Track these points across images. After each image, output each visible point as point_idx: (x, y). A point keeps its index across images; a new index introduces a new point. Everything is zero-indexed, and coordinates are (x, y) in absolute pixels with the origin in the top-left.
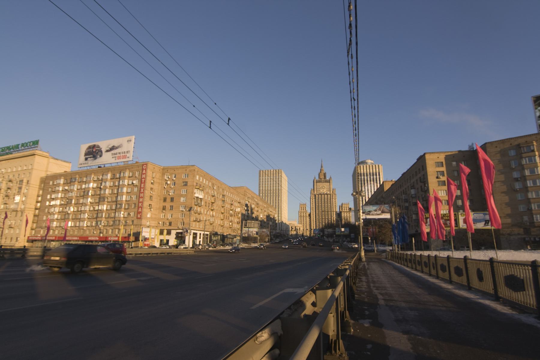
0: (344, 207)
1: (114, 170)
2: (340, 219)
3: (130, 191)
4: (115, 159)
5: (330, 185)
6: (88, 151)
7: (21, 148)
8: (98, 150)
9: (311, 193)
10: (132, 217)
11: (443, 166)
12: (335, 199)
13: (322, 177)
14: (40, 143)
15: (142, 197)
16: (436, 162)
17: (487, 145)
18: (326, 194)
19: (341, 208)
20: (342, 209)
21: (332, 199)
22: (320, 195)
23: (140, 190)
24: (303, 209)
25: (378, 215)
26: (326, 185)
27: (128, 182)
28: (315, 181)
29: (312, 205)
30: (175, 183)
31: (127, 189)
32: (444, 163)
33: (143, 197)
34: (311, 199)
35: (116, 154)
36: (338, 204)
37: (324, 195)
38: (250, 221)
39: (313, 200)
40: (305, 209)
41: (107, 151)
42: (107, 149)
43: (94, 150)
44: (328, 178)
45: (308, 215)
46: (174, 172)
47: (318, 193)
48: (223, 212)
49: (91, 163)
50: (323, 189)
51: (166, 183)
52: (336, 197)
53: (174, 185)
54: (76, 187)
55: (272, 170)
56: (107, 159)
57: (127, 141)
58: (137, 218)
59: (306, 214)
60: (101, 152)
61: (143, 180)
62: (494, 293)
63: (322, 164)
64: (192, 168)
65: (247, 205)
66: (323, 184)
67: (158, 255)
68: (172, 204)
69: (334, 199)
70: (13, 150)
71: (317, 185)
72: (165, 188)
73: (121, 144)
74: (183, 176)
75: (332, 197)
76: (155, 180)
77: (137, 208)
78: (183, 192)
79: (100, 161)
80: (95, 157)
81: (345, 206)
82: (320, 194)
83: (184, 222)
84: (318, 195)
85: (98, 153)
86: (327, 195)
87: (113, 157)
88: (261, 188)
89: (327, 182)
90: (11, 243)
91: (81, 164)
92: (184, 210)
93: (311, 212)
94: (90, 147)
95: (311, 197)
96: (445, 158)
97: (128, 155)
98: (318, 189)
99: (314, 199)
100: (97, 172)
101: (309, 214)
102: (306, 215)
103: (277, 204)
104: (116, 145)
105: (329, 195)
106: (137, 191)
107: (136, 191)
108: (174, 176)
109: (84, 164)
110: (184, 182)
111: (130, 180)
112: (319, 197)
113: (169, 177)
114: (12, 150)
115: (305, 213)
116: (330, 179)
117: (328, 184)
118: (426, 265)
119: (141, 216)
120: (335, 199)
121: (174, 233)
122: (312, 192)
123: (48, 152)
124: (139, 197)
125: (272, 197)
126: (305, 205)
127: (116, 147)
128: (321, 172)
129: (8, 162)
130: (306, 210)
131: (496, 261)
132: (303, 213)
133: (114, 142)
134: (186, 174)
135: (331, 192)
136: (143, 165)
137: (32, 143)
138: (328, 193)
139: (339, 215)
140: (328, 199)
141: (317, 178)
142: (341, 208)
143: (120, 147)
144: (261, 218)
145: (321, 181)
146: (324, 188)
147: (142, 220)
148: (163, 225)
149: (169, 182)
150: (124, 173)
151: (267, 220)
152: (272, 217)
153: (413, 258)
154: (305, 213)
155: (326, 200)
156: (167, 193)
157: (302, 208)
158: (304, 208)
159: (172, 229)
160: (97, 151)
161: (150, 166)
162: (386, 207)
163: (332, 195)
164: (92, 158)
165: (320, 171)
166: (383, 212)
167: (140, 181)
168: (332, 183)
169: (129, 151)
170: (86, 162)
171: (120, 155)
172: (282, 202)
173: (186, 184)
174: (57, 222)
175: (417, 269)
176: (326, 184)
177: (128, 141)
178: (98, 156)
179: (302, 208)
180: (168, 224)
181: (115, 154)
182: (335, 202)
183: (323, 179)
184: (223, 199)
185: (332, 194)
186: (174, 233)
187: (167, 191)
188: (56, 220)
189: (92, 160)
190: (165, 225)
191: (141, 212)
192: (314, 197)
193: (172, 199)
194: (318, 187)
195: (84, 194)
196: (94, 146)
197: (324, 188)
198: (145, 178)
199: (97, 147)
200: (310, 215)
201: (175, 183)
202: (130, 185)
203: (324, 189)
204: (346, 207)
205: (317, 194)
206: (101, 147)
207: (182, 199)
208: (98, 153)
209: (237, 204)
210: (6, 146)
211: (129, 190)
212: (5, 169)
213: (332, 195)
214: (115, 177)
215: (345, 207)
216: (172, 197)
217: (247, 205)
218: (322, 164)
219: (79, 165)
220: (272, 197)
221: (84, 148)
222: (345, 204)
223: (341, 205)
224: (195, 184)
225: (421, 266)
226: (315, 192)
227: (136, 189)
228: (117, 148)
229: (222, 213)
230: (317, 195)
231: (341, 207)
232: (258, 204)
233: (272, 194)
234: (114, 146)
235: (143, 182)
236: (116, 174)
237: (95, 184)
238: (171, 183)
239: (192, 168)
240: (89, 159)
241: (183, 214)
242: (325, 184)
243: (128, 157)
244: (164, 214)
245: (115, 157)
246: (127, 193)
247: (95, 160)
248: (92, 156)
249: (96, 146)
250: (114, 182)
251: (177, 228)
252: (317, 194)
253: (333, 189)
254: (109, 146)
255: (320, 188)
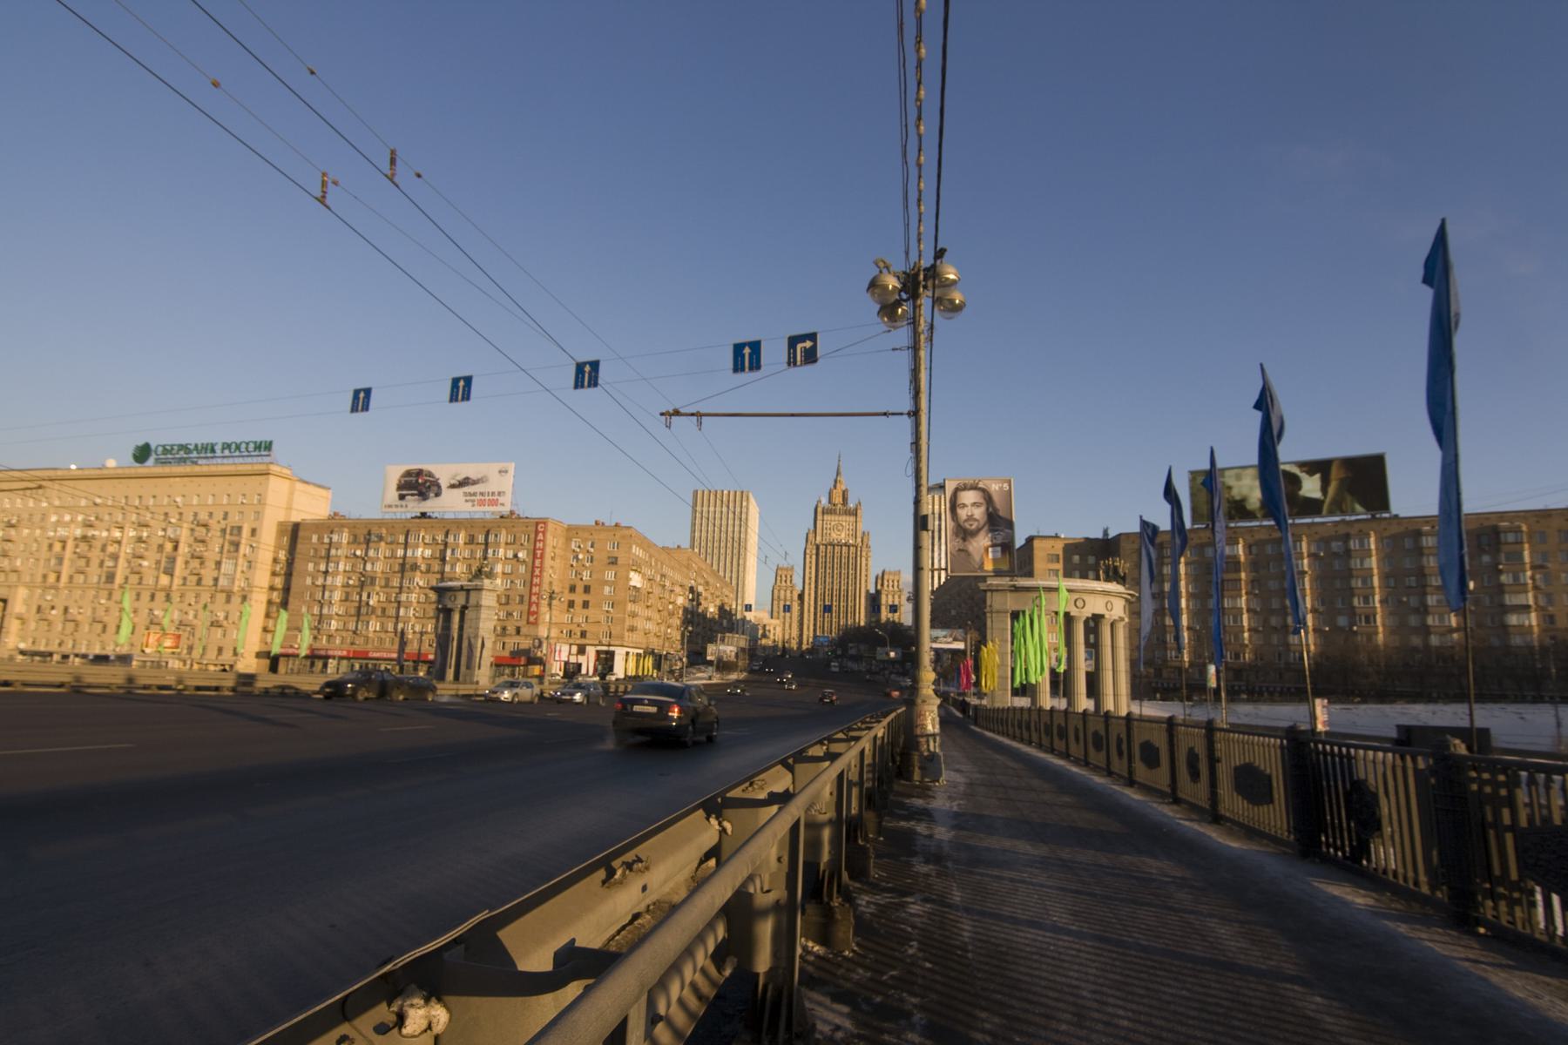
0: (888, 581)
1: (472, 527)
2: (944, 755)
3: (509, 572)
4: (473, 506)
5: (856, 522)
6: (405, 481)
7: (222, 452)
8: (431, 482)
9: (807, 541)
10: (517, 620)
11: (1058, 562)
12: (867, 560)
13: (838, 500)
14: (274, 447)
15: (536, 585)
16: (1049, 554)
17: (1122, 537)
18: (845, 545)
19: (880, 582)
20: (882, 585)
21: (859, 558)
22: (829, 547)
23: (533, 572)
24: (786, 581)
25: (949, 643)
26: (846, 521)
27: (505, 553)
28: (820, 510)
29: (807, 570)
30: (592, 557)
31: (504, 567)
32: (1061, 557)
33: (539, 585)
34: (808, 556)
35: (474, 494)
36: (874, 570)
37: (841, 546)
38: (731, 635)
39: (811, 557)
40: (791, 581)
41: (453, 486)
42: (453, 482)
43: (420, 481)
44: (851, 505)
45: (796, 597)
46: (591, 537)
47: (824, 542)
48: (661, 609)
49: (413, 507)
50: (839, 530)
51: (576, 557)
52: (870, 554)
53: (591, 562)
54: (384, 551)
55: (725, 492)
56: (450, 504)
57: (497, 471)
58: (528, 622)
59: (791, 592)
60: (439, 487)
61: (539, 552)
62: (1446, 900)
63: (839, 466)
64: (627, 532)
65: (692, 590)
66: (840, 518)
67: (221, 693)
68: (586, 597)
69: (863, 559)
70: (197, 455)
71: (823, 520)
72: (572, 566)
73: (485, 477)
74: (609, 547)
75: (859, 553)
76: (556, 551)
77: (526, 603)
78: (609, 575)
79: (432, 506)
80: (423, 496)
81: (891, 577)
82: (830, 545)
83: (610, 633)
84: (826, 546)
85: (429, 487)
86: (849, 546)
87: (467, 501)
88: (697, 534)
89: (850, 515)
90: (220, 658)
91: (390, 506)
92: (610, 609)
93: (804, 588)
94: (408, 473)
95: (808, 551)
96: (1064, 548)
97: (501, 500)
98: (825, 531)
99: (814, 557)
100: (432, 527)
101: (799, 592)
102: (791, 597)
103: (734, 576)
104: (473, 476)
105: (851, 548)
106: (526, 571)
107: (524, 572)
108: (590, 544)
109: (397, 506)
110: (609, 558)
111: (510, 549)
112: (826, 552)
113: (582, 546)
114: (195, 454)
115: (788, 592)
116: (857, 506)
117: (852, 519)
118: (1099, 742)
119: (536, 619)
120: (867, 560)
121: (591, 651)
122: (811, 536)
123: (289, 467)
124: (531, 585)
125: (722, 558)
126: (792, 568)
127: (474, 481)
128: (835, 487)
129: (192, 481)
130: (793, 582)
131: (1136, 717)
132: (785, 591)
133: (471, 471)
134: (614, 544)
135: (859, 540)
136: (537, 524)
137: (252, 446)
138: (851, 541)
139: (874, 601)
140: (848, 557)
141: (824, 501)
142: (880, 582)
143: (483, 482)
144: (711, 613)
145: (835, 510)
146: (840, 528)
147: (537, 627)
148: (570, 636)
149: (581, 556)
150: (496, 536)
151: (720, 616)
152: (728, 609)
153: (1034, 716)
154: (788, 592)
155: (843, 560)
156: (576, 575)
157: (784, 578)
158: (789, 576)
159: (589, 645)
160: (428, 484)
161: (550, 527)
162: (959, 633)
163: (859, 549)
164: (416, 497)
165: (833, 483)
166: (955, 639)
167: (532, 554)
168: (861, 517)
169: (504, 492)
170: (403, 503)
171: (483, 498)
172: (747, 569)
173: (613, 562)
174: (338, 621)
175: (1181, 795)
176: (848, 518)
177: (500, 472)
178: (432, 495)
179: (784, 578)
180: (579, 634)
181: (470, 494)
182: (867, 565)
183: (839, 506)
184: (662, 583)
185: (860, 544)
186: (591, 651)
187: (576, 572)
188: (336, 617)
189: (414, 500)
190: (573, 636)
191: (536, 613)
192: (814, 552)
193: (587, 589)
194: (825, 526)
195: (406, 567)
196: (420, 473)
197: (840, 528)
198: (543, 550)
199: (426, 475)
200: (801, 597)
201: (592, 557)
202: (509, 559)
203: (839, 530)
204: (893, 581)
205: (823, 545)
206: (437, 477)
207: (607, 589)
208: (429, 487)
209: (678, 589)
210: (177, 443)
211: (508, 569)
212: (184, 496)
213: (861, 548)
214: (475, 541)
215: (890, 581)
216: (586, 584)
217: (692, 590)
218: (839, 466)
219: (385, 506)
220: (722, 558)
221: (395, 474)
222: (890, 573)
223: (880, 575)
224: (631, 562)
225: (1064, 741)
226: (819, 538)
227: (522, 569)
228: (475, 483)
229: (659, 611)
230: (821, 547)
231: (881, 578)
232: (707, 583)
233: (722, 551)
234: (467, 478)
235: (539, 556)
236: (476, 535)
237: (427, 550)
238: (584, 558)
239: (627, 532)
240: (408, 498)
241: (608, 617)
242: (844, 518)
243: (503, 505)
244: (570, 616)
245: (473, 501)
246: (504, 573)
247: (424, 503)
248: (415, 492)
249: (424, 473)
250: (472, 551)
251: (597, 642)
252: (823, 545)
253: (864, 533)
254: (456, 476)
255: (830, 529)
